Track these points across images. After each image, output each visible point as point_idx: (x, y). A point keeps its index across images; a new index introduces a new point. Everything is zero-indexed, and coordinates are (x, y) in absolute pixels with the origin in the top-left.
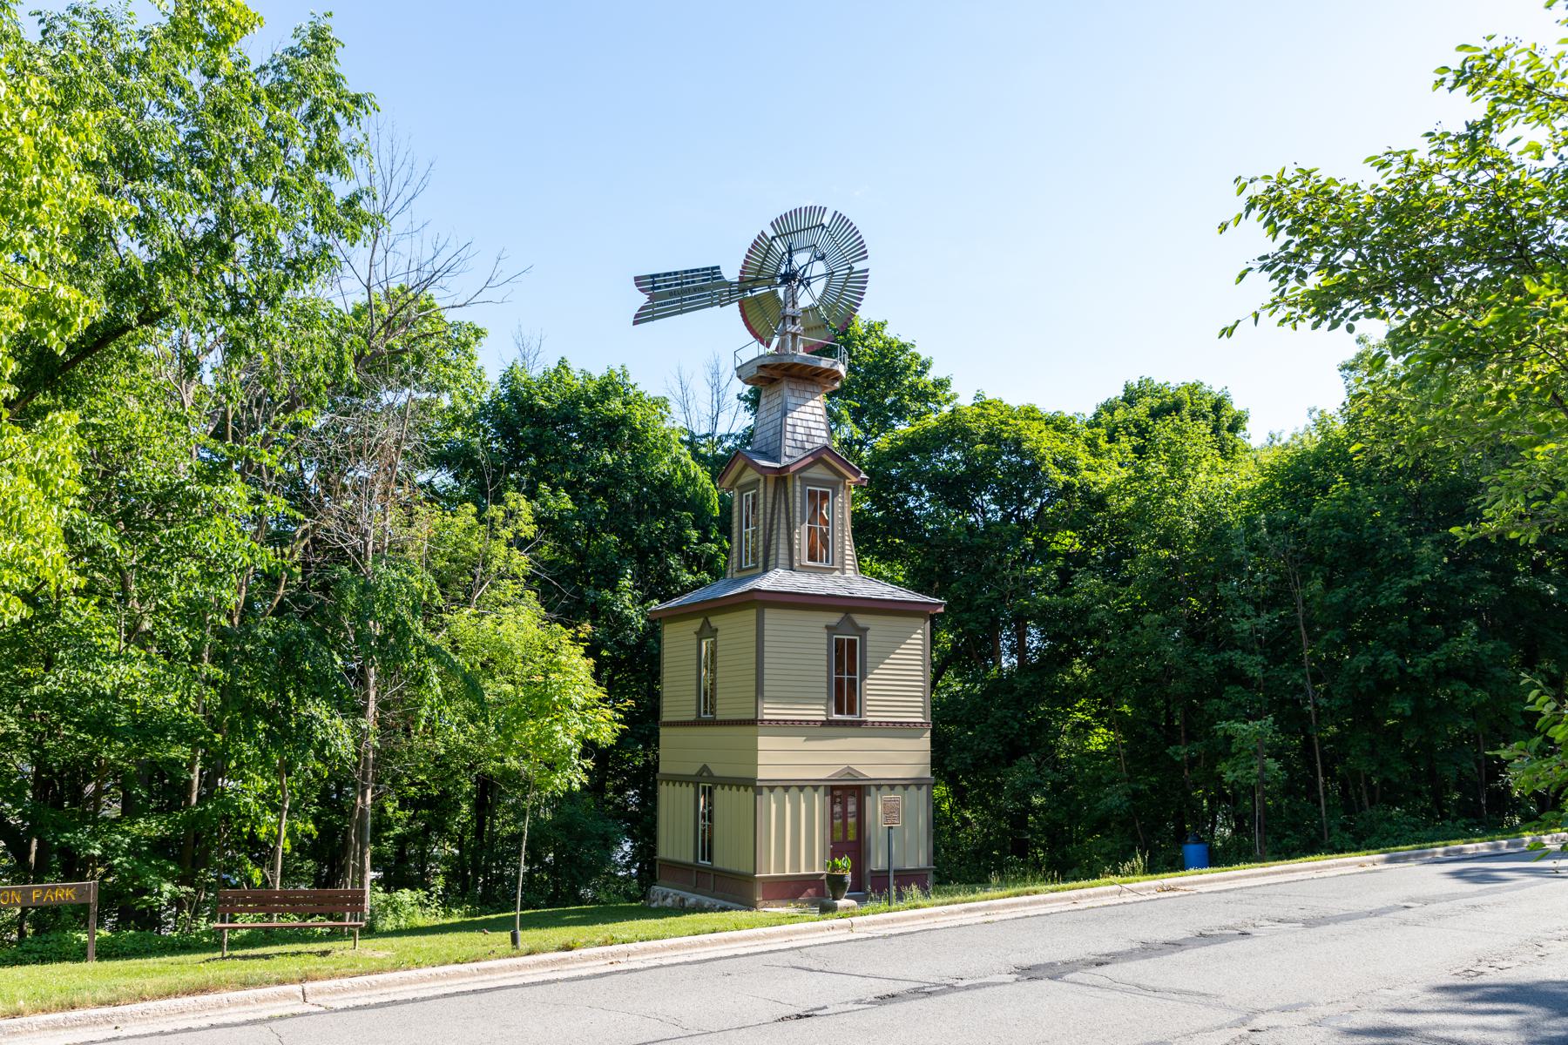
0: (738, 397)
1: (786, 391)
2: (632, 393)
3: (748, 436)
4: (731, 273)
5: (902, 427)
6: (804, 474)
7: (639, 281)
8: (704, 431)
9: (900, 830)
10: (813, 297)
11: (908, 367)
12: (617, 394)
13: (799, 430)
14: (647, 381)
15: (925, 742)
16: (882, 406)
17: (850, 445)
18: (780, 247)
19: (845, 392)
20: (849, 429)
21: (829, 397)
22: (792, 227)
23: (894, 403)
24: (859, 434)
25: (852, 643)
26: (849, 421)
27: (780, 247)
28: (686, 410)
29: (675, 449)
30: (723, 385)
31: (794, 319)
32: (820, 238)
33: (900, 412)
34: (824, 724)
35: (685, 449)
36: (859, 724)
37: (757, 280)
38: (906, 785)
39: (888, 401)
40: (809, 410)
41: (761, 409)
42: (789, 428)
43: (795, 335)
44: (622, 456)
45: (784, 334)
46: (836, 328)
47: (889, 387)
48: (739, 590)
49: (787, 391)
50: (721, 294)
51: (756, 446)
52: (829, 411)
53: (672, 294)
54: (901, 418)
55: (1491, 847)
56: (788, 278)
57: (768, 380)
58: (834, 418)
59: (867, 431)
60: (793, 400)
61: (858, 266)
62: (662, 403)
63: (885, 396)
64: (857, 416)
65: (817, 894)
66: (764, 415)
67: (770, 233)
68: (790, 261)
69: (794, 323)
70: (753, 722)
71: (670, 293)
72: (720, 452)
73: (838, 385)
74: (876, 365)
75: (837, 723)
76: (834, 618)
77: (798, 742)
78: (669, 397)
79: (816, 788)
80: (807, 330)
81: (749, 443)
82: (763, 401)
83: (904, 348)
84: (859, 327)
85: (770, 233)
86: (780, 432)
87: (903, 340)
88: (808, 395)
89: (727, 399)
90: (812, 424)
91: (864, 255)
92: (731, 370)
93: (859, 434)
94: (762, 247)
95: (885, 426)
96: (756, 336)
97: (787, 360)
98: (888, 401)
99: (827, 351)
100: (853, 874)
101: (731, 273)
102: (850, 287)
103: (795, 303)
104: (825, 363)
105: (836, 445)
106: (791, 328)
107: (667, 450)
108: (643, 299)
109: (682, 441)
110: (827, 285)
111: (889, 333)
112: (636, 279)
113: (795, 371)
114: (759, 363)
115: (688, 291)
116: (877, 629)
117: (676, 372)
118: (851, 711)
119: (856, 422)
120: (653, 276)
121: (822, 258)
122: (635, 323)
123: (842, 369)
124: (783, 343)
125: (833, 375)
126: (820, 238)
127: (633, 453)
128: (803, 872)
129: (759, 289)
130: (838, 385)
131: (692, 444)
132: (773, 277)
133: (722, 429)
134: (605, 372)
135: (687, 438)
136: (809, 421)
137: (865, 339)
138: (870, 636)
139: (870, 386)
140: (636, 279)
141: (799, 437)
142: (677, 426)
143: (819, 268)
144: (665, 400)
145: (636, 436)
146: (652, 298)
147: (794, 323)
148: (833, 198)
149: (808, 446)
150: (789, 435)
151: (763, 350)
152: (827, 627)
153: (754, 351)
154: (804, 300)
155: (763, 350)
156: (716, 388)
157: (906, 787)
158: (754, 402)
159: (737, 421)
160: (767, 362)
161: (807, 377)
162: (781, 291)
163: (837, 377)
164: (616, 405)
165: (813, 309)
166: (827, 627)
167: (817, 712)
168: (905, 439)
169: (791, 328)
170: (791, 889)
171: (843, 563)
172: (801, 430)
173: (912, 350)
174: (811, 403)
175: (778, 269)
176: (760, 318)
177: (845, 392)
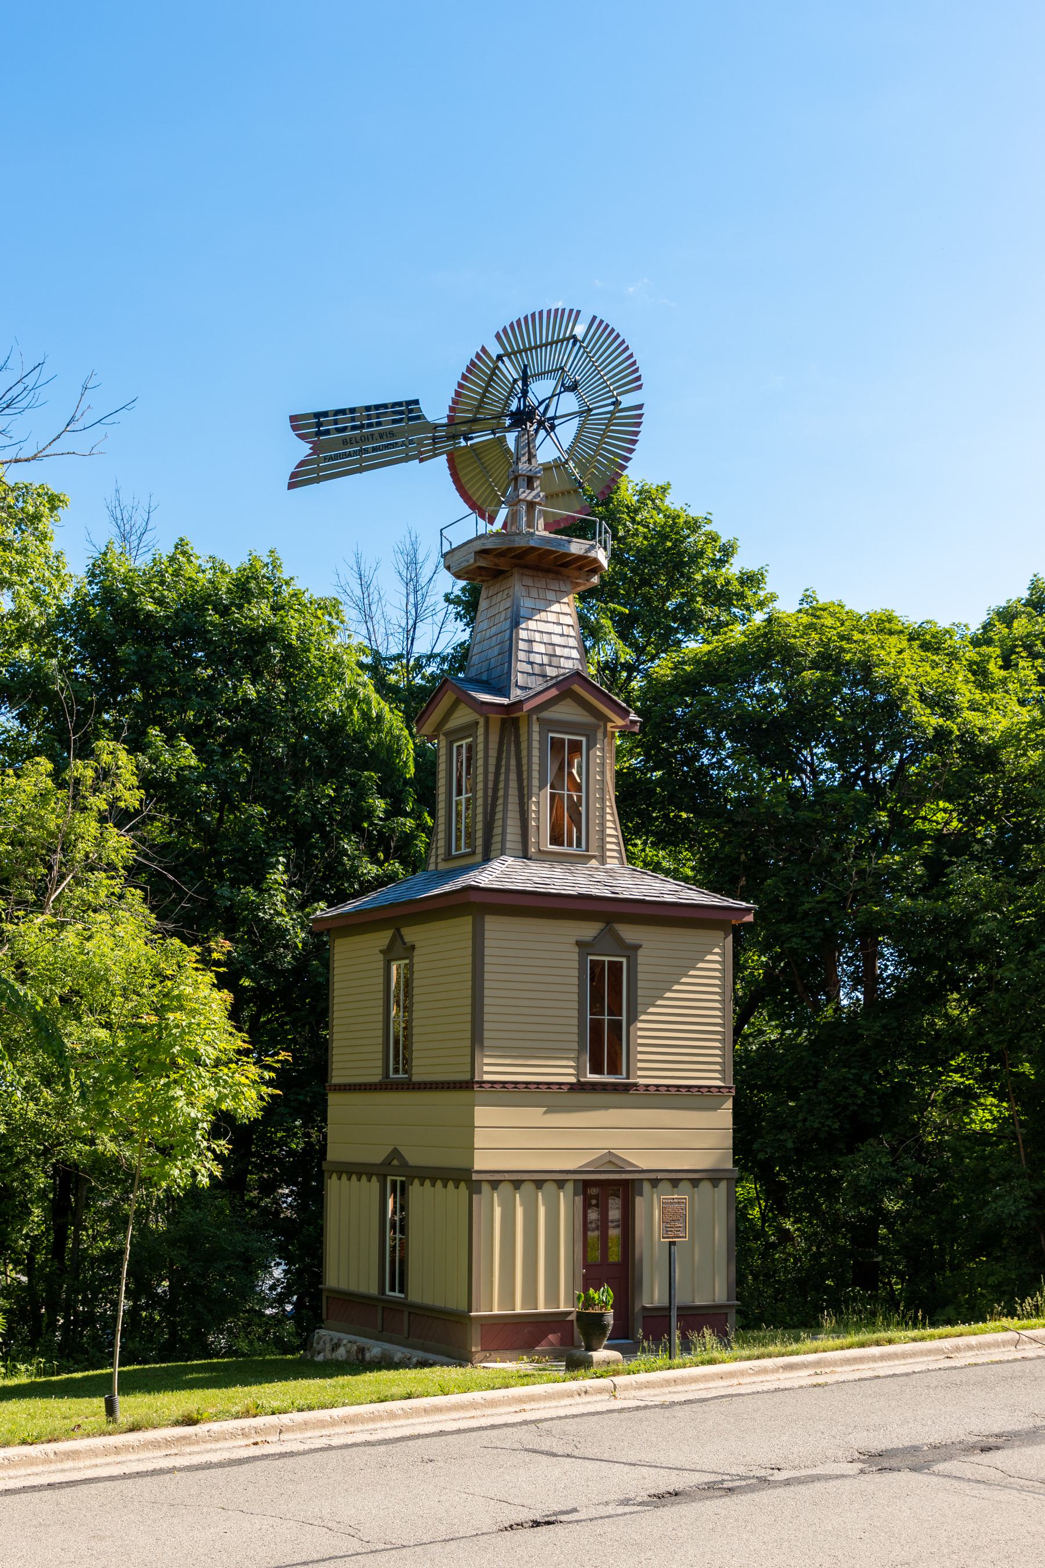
6: (546, 714)
9: (688, 1249)
15: (724, 1116)
25: (616, 967)
34: (573, 1088)
36: (626, 1088)
38: (695, 1179)
40: (551, 617)
53: (346, 442)
65: (562, 1342)
75: (594, 1087)
76: (589, 930)
77: (534, 1115)
79: (561, 1184)
88: (550, 595)
100: (617, 1314)
115: (365, 439)
116: (653, 945)
118: (614, 1070)
128: (542, 1309)
138: (642, 957)
152: (579, 944)
157: (695, 1183)
166: (579, 944)
167: (562, 1071)
170: (523, 1335)
171: (603, 848)
174: (556, 607)
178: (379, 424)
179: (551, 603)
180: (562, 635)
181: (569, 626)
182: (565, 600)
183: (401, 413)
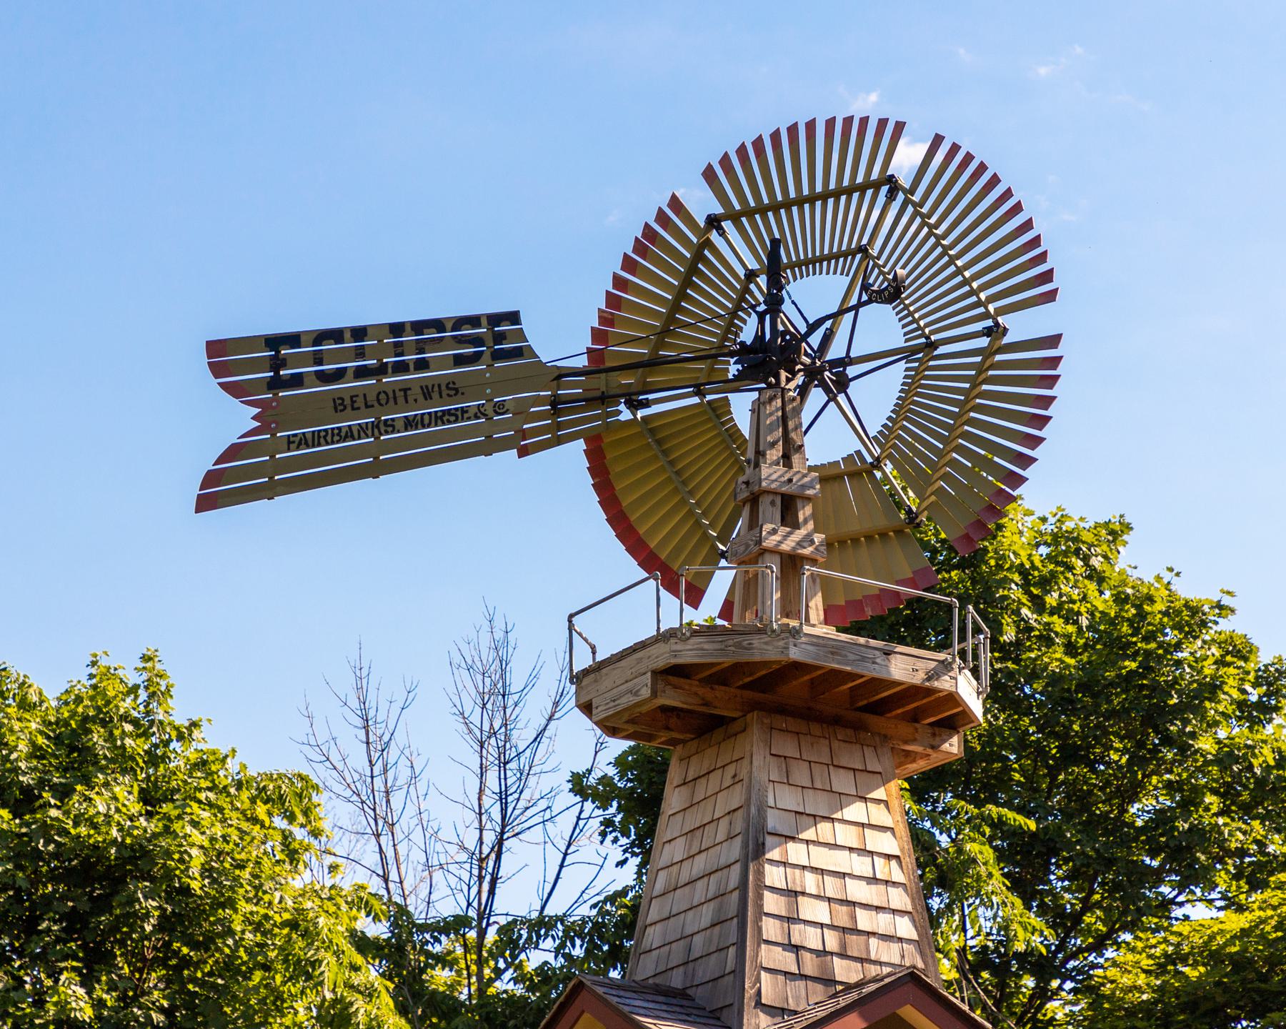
0: (578, 785)
1: (762, 766)
2: (181, 756)
3: (614, 931)
4: (561, 334)
5: (1199, 912)
7: (222, 356)
8: (447, 908)
10: (856, 425)
11: (1212, 689)
12: (124, 762)
13: (813, 910)
14: (240, 718)
16: (1118, 828)
17: (1002, 972)
18: (737, 251)
19: (976, 777)
20: (997, 913)
21: (920, 789)
22: (789, 185)
23: (1161, 819)
24: (1032, 933)
26: (997, 883)
27: (737, 251)
28: (382, 824)
29: (330, 971)
30: (522, 737)
31: (788, 507)
32: (879, 220)
33: (1189, 857)
35: (371, 974)
37: (653, 363)
39: (1139, 811)
40: (846, 835)
41: (668, 827)
42: (772, 903)
43: (792, 563)
44: (131, 995)
45: (750, 556)
46: (944, 541)
47: (1142, 758)
48: (750, 908)
49: (766, 769)
50: (522, 411)
51: (646, 968)
52: (921, 842)
53: (341, 405)
54: (1194, 877)
55: (749, 647)
56: (770, 360)
57: (690, 726)
58: (940, 875)
59: (1066, 923)
60: (786, 798)
61: (1019, 326)
62: (288, 797)
63: (1132, 792)
64: (1026, 863)
66: (676, 851)
67: (702, 203)
68: (774, 303)
69: (788, 517)
70: (793, 838)
71: (336, 403)
72: (505, 985)
73: (953, 746)
74: (1090, 683)
78: (319, 774)
80: (838, 545)
81: (617, 956)
82: (673, 799)
83: (1191, 619)
84: (1018, 538)
85: (702, 203)
86: (738, 915)
87: (1187, 590)
88: (842, 782)
89: (536, 787)
90: (858, 891)
91: (1041, 287)
92: (552, 680)
93: (1032, 933)
94: (667, 251)
95: (1134, 908)
96: (649, 560)
97: (765, 651)
98: (1139, 811)
99: (913, 623)
101: (561, 334)
102: (989, 399)
103: (791, 450)
104: (905, 666)
105: (947, 970)
106: (778, 538)
107: (305, 971)
108: (239, 419)
109: (362, 944)
110: (910, 388)
111: (1138, 562)
112: (215, 348)
113: (794, 689)
114: (662, 656)
117: (346, 686)
119: (1024, 887)
120: (274, 342)
121: (892, 293)
122: (205, 503)
123: (967, 690)
124: (747, 590)
125: (931, 711)
126: (879, 220)
127: (174, 980)
129: (658, 396)
130: (953, 746)
131: (400, 951)
132: (714, 355)
133: (515, 901)
134: (80, 678)
135: (378, 930)
136: (846, 871)
137: (1047, 582)
139: (1071, 755)
140: (215, 348)
141: (811, 938)
142: (347, 880)
143: (880, 328)
144: (305, 788)
145: (189, 918)
146: (266, 420)
147: (788, 517)
148: (925, 97)
149: (845, 971)
150: (771, 929)
151: (673, 612)
153: (638, 614)
154: (828, 439)
155: (673, 612)
156: (498, 750)
158: (635, 806)
159: (569, 869)
160: (688, 654)
161: (839, 717)
162: (741, 406)
163: (950, 716)
164: (112, 806)
165: (856, 471)
168: (1214, 957)
169: (778, 538)
172: (819, 912)
173: (1225, 625)
174: (855, 811)
175: (731, 328)
176: (666, 496)
177: (976, 777)
178: (422, 365)
179: (842, 799)
180: (873, 880)
181: (889, 857)
182: (880, 793)
183: (477, 341)
